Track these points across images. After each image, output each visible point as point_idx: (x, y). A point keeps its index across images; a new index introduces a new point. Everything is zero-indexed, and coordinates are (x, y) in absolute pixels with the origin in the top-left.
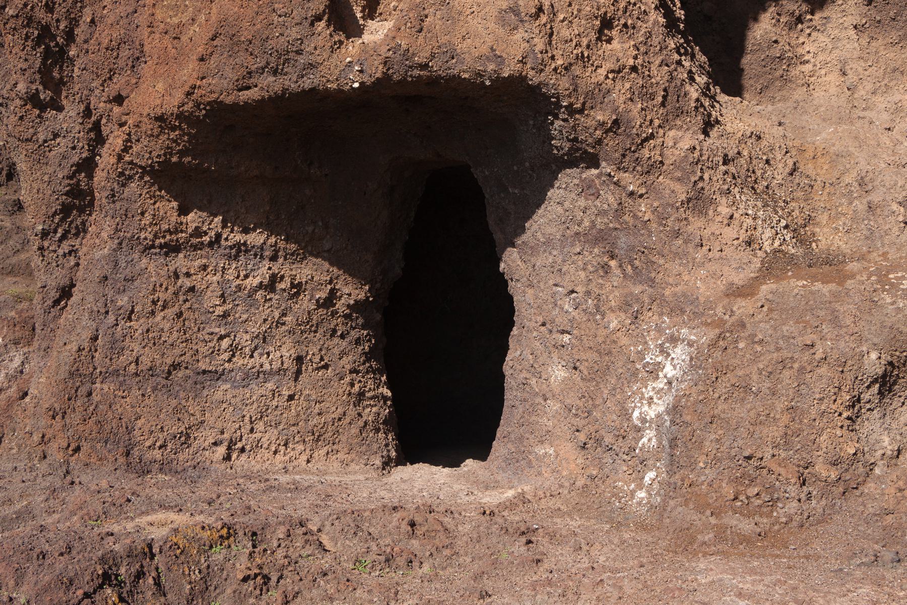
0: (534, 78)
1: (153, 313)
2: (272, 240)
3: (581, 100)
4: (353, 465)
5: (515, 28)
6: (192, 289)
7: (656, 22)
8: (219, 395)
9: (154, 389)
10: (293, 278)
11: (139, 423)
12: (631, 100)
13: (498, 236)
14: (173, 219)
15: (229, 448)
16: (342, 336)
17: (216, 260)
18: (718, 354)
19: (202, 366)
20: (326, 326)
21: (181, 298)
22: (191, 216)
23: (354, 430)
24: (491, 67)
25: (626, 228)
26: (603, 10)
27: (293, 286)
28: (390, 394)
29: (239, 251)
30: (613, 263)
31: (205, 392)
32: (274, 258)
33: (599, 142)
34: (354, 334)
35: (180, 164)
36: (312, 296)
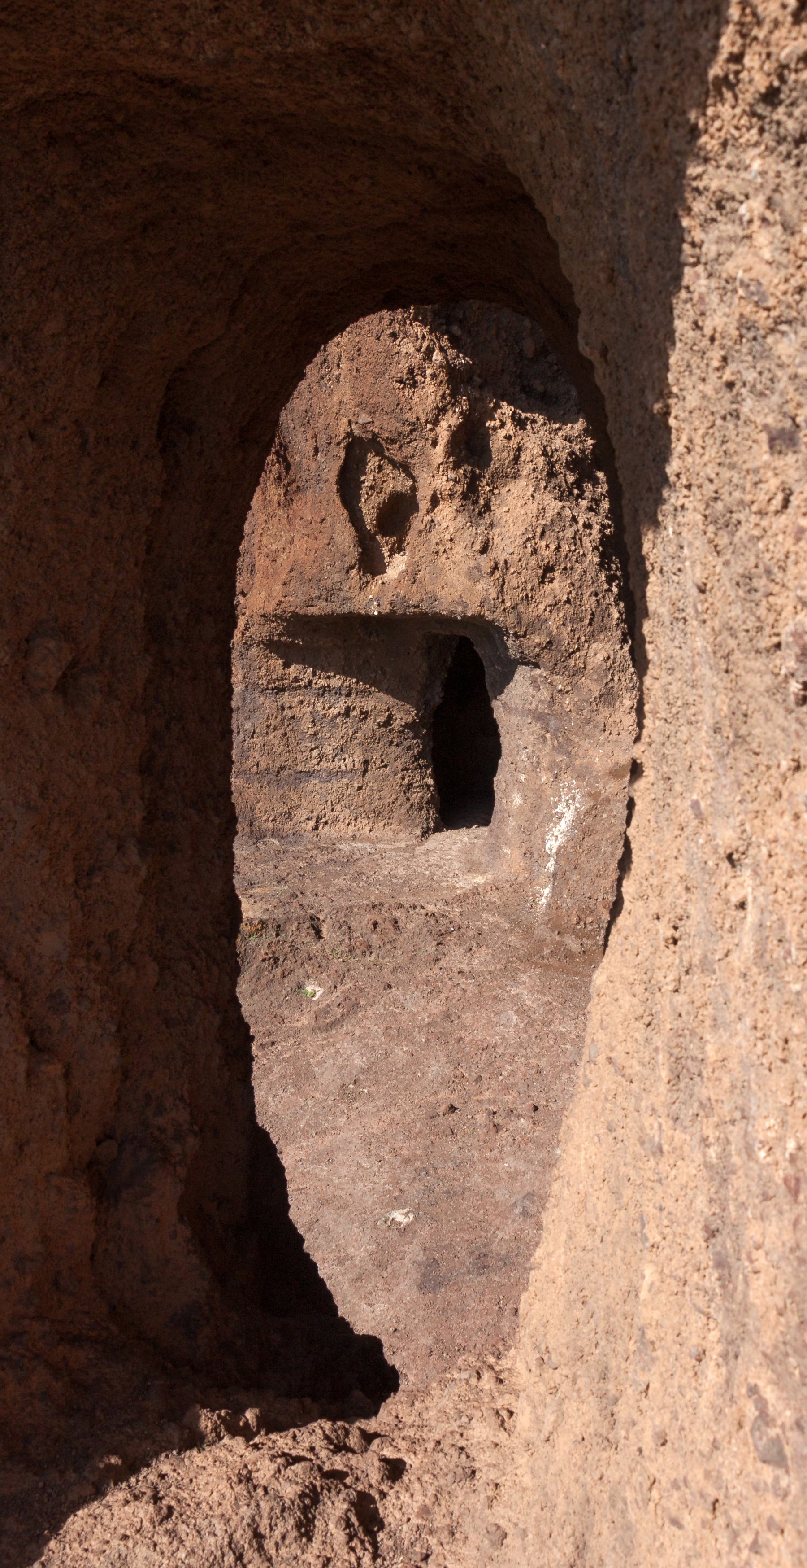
0: (489, 616)
1: (267, 733)
3: (524, 629)
4: (401, 834)
5: (478, 581)
6: (293, 717)
7: (591, 562)
8: (311, 787)
9: (268, 783)
10: (362, 708)
11: (259, 805)
12: (564, 624)
13: (490, 694)
14: (280, 672)
15: (317, 822)
16: (398, 745)
17: (310, 698)
18: (590, 820)
19: (300, 768)
20: (385, 739)
21: (286, 723)
22: (292, 668)
23: (403, 811)
24: (460, 609)
25: (555, 715)
26: (546, 561)
27: (362, 713)
28: (432, 783)
29: (325, 691)
30: (548, 735)
31: (302, 785)
32: (349, 695)
33: (538, 655)
34: (406, 743)
35: (279, 641)
36: (375, 720)
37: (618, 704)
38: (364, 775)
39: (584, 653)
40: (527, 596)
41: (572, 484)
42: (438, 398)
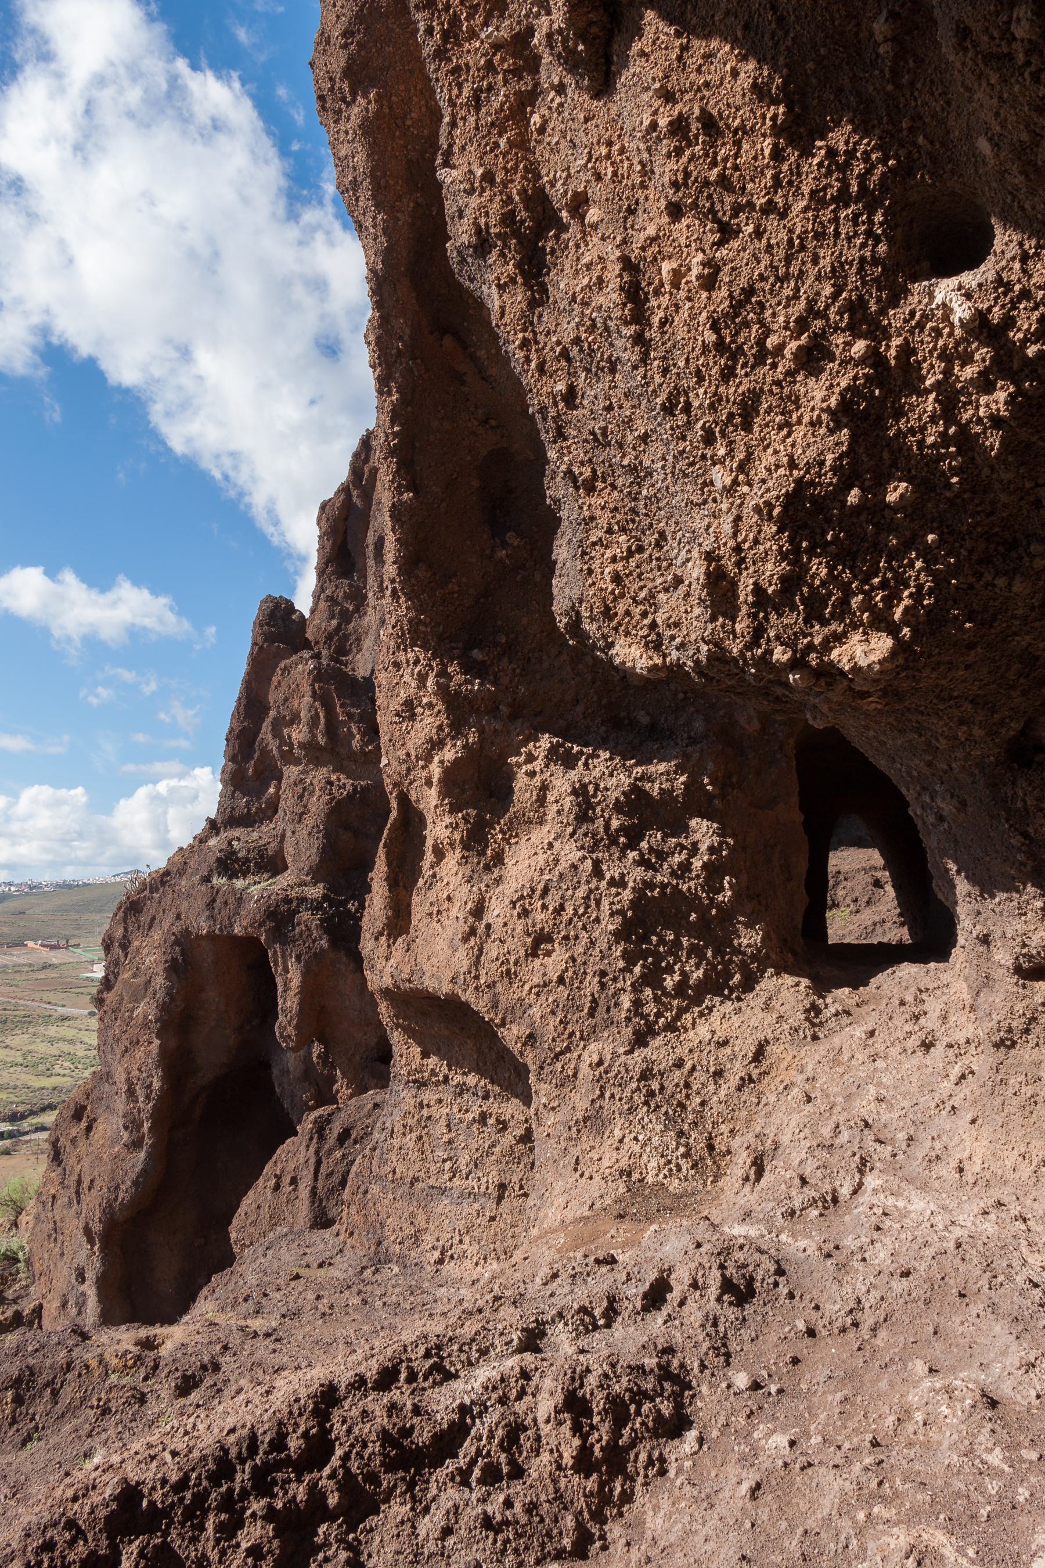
1: (404, 1134)
2: (482, 1083)
3: (500, 1016)
6: (429, 1118)
11: (389, 1221)
12: (553, 1013)
15: (442, 1253)
19: (431, 1182)
26: (539, 927)
32: (486, 1097)
37: (607, 1133)
38: (499, 1202)
39: (576, 1054)
40: (508, 971)
41: (617, 831)
42: (434, 730)
